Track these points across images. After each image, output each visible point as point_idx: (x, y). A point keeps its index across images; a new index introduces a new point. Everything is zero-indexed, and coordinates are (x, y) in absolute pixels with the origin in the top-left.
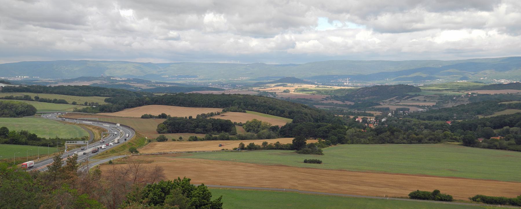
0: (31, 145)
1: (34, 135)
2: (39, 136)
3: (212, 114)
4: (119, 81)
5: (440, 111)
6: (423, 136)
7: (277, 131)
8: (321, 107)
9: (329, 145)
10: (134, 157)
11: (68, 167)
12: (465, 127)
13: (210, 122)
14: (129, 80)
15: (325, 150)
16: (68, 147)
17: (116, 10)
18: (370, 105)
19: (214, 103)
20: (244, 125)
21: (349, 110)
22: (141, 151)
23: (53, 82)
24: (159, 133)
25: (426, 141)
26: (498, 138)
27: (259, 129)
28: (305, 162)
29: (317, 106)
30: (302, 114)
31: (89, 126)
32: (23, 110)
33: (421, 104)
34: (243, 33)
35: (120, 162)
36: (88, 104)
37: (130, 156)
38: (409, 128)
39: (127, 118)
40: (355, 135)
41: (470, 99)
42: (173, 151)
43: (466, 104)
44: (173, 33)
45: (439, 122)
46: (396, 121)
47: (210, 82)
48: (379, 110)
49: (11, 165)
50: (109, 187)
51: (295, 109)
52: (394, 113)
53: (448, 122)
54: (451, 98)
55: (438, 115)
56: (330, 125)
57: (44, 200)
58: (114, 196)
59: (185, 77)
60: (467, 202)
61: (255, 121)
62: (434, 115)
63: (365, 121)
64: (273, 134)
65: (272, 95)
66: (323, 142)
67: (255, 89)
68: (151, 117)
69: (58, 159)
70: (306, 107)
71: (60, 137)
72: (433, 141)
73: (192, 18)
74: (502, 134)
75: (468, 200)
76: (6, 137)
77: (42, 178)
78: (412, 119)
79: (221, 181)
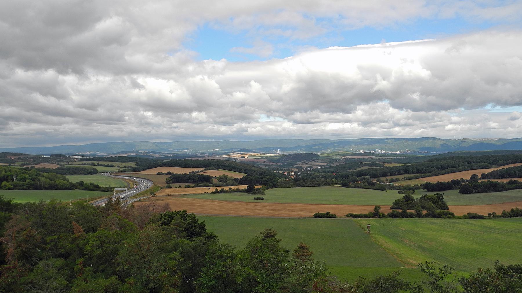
0: (96, 191)
1: (97, 185)
2: (100, 186)
3: (198, 172)
5: (329, 168)
6: (320, 182)
7: (237, 181)
8: (263, 167)
9: (268, 188)
10: (153, 197)
11: (115, 204)
12: (343, 177)
13: (197, 176)
14: (149, 152)
15: (266, 192)
16: (116, 192)
17: (142, 112)
18: (292, 165)
19: (199, 165)
20: (218, 178)
21: (280, 168)
22: (157, 194)
23: (107, 154)
25: (322, 185)
26: (359, 182)
27: (227, 180)
28: (255, 199)
29: (261, 166)
30: (252, 171)
31: (127, 179)
32: (91, 171)
33: (320, 164)
34: (216, 123)
35: (145, 200)
36: (126, 167)
37: (150, 197)
38: (313, 178)
39: (148, 174)
40: (283, 183)
41: (345, 161)
42: (175, 194)
43: (343, 164)
44: (175, 125)
45: (330, 174)
46: (306, 174)
47: (197, 153)
48: (297, 168)
49: (86, 202)
50: (139, 215)
51: (248, 168)
52: (305, 169)
53: (334, 174)
54: (335, 161)
55: (329, 170)
56: (269, 177)
57: (103, 222)
58: (142, 220)
59: (182, 149)
60: (344, 218)
61: (224, 175)
62: (326, 170)
63: (288, 174)
64: (235, 183)
65: (235, 159)
66: (265, 187)
67: (225, 156)
68: (162, 174)
69: (110, 199)
70: (254, 167)
71: (111, 186)
72: (326, 185)
73: (186, 115)
74: (361, 180)
75: (344, 216)
76: (83, 186)
77: (102, 209)
78: (315, 173)
79: (204, 211)
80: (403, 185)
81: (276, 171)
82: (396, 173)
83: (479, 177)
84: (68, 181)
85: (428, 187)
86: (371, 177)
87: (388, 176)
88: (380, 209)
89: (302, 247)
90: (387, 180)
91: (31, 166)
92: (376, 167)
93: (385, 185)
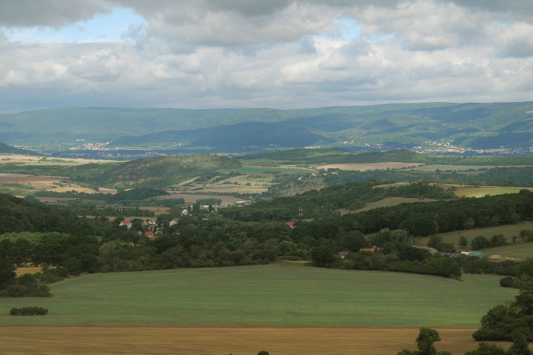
9: (63, 275)
15: (55, 288)
25: (249, 260)
26: (372, 250)
28: (14, 312)
41: (327, 180)
43: (318, 190)
46: (196, 224)
48: (167, 203)
55: (271, 209)
62: (264, 210)
63: (137, 225)
66: (52, 271)
80: (519, 260)
81: (93, 217)
82: (496, 219)
86: (410, 233)
87: (468, 228)
88: (434, 340)
90: (464, 244)
92: (426, 200)
93: (458, 259)
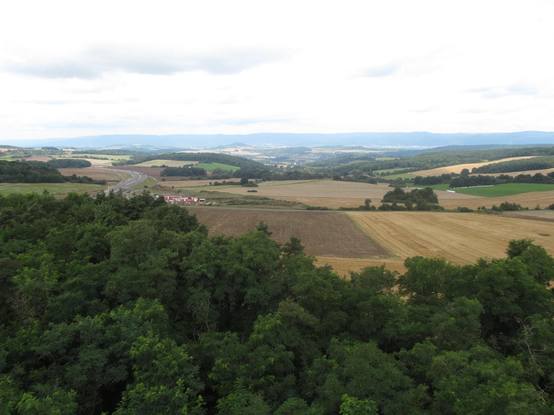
4: (137, 146)
9: (261, 182)
24: (161, 176)
28: (249, 191)
33: (312, 158)
61: (520, 175)
83: (470, 171)
84: (60, 174)
85: (418, 181)
89: (295, 241)
91: (21, 159)
